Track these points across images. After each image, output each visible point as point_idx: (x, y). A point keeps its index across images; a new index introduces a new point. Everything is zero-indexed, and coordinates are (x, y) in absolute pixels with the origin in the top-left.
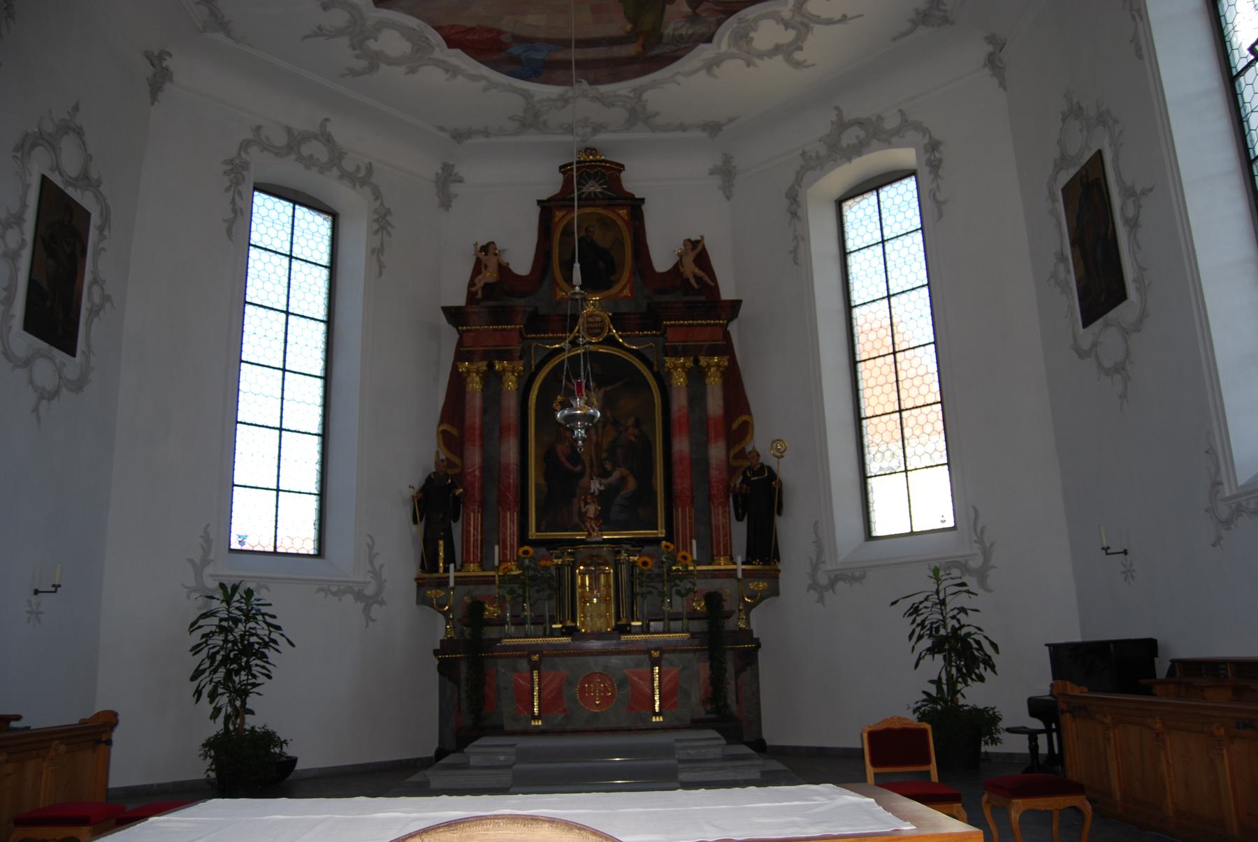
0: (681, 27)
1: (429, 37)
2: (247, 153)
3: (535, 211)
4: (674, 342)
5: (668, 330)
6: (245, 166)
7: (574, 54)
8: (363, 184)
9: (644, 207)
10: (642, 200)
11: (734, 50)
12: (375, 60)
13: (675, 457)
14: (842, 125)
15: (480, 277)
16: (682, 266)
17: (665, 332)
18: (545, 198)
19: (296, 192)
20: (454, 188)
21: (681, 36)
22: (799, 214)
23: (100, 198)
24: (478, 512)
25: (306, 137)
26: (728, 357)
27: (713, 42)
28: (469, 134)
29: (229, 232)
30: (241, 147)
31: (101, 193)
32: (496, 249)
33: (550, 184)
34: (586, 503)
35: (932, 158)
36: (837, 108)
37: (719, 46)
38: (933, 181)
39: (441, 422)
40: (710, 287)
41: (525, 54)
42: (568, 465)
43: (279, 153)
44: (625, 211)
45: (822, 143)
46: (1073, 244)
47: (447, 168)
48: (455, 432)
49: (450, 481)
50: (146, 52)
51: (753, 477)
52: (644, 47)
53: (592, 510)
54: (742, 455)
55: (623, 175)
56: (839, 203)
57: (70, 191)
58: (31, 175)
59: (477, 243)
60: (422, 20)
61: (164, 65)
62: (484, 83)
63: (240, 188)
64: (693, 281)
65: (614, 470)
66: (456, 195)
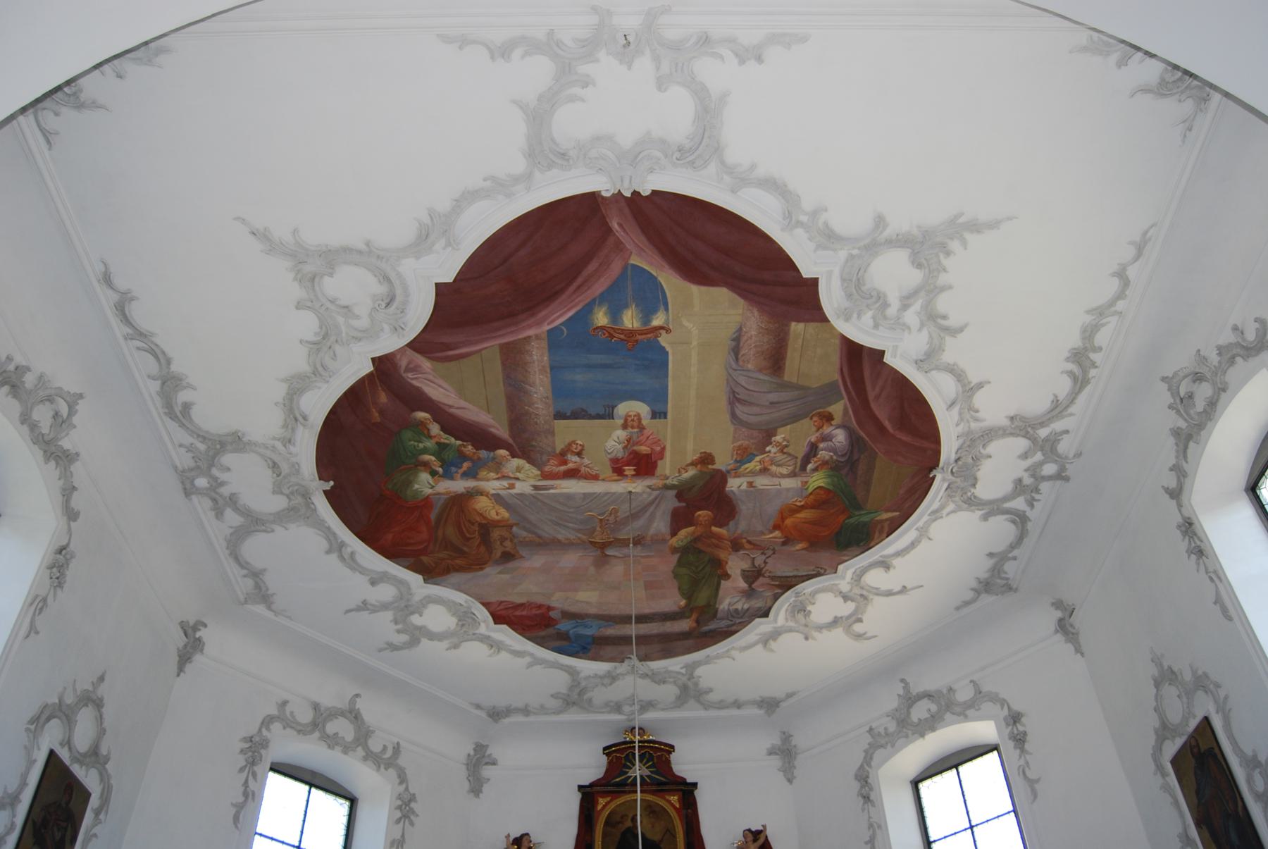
0: (736, 602)
1: (475, 612)
2: (268, 729)
3: (575, 800)
6: (265, 744)
7: (633, 630)
8: (388, 765)
9: (696, 793)
10: (695, 785)
11: (791, 624)
12: (417, 635)
14: (910, 700)
18: (587, 784)
19: (314, 773)
20: (487, 771)
21: (736, 610)
22: (871, 798)
23: (104, 777)
25: (334, 714)
27: (770, 616)
28: (508, 712)
29: (236, 819)
30: (262, 723)
31: (106, 771)
32: (531, 842)
33: (592, 767)
35: (1016, 732)
36: (902, 681)
37: (775, 621)
38: (1020, 757)
41: (575, 630)
43: (302, 730)
44: (676, 798)
45: (890, 718)
46: (1198, 824)
47: (480, 748)
50: (183, 622)
52: (697, 622)
55: (673, 757)
56: (915, 784)
57: (77, 770)
58: (39, 749)
59: (509, 835)
60: (471, 596)
61: (197, 636)
62: (528, 659)
63: (256, 768)
66: (489, 780)
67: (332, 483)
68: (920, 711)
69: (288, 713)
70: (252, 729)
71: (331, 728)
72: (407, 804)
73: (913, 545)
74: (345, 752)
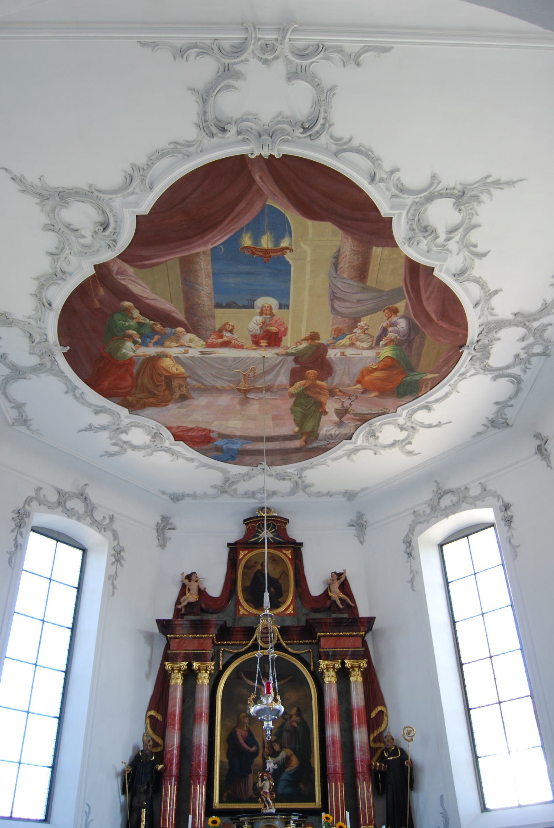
2: (29, 505)
4: (326, 649)
5: (322, 640)
7: (264, 446)
9: (302, 549)
10: (301, 544)
13: (329, 740)
15: (184, 597)
16: (330, 591)
17: (319, 640)
19: (59, 533)
21: (331, 435)
24: (175, 785)
26: (367, 660)
32: (197, 577)
34: (263, 780)
36: (436, 482)
38: (508, 531)
39: (149, 710)
40: (352, 608)
41: (226, 445)
42: (246, 746)
43: (51, 507)
48: (159, 717)
49: (153, 758)
51: (389, 757)
52: (306, 442)
53: (267, 785)
54: (379, 738)
55: (288, 526)
56: (441, 546)
59: (183, 573)
63: (22, 530)
64: (338, 602)
65: (281, 751)
67: (68, 348)
68: (446, 501)
69: (42, 496)
70: (20, 505)
71: (70, 504)
72: (119, 553)
73: (446, 395)
74: (79, 519)
